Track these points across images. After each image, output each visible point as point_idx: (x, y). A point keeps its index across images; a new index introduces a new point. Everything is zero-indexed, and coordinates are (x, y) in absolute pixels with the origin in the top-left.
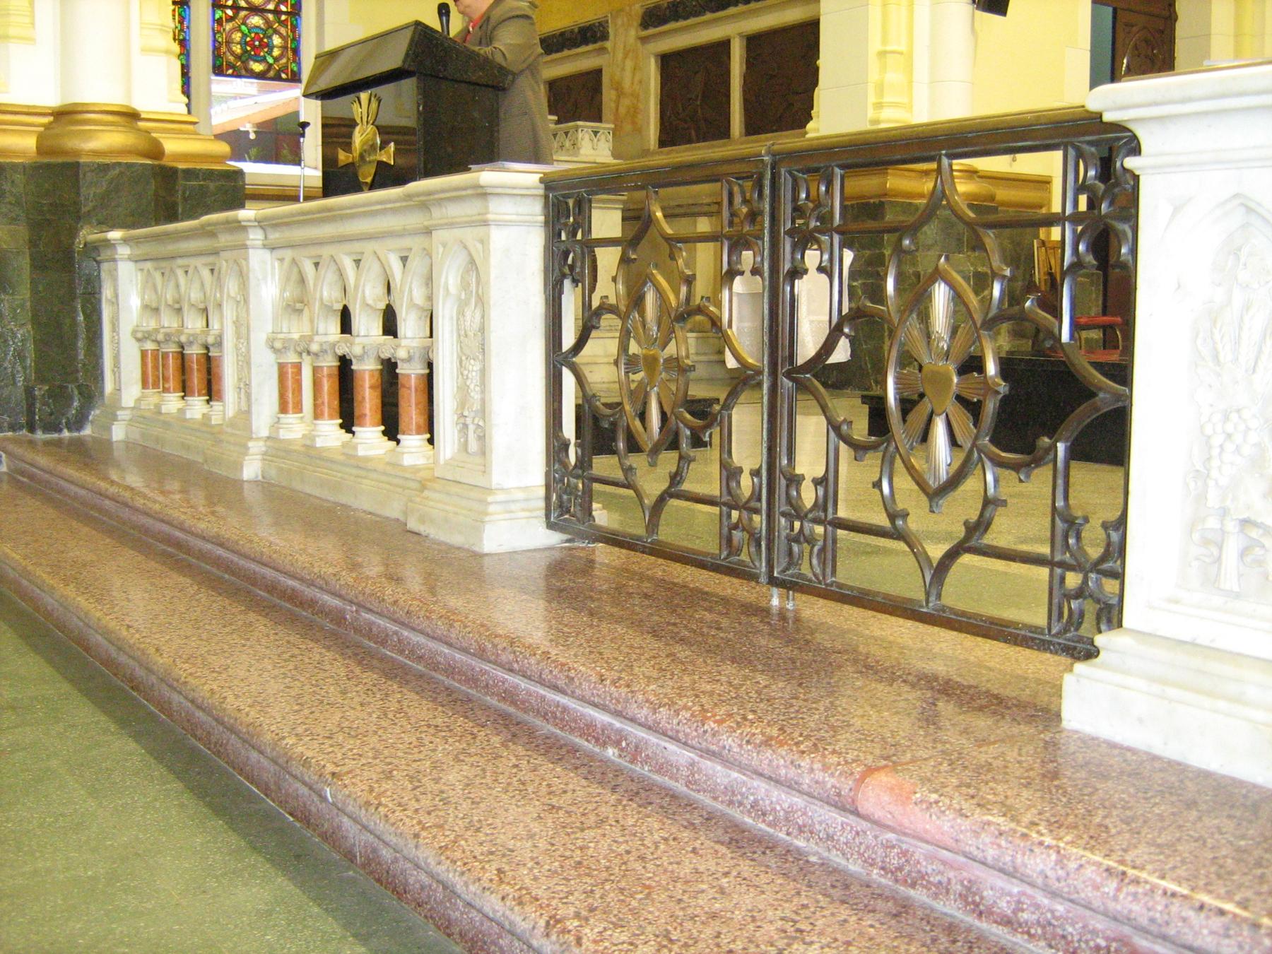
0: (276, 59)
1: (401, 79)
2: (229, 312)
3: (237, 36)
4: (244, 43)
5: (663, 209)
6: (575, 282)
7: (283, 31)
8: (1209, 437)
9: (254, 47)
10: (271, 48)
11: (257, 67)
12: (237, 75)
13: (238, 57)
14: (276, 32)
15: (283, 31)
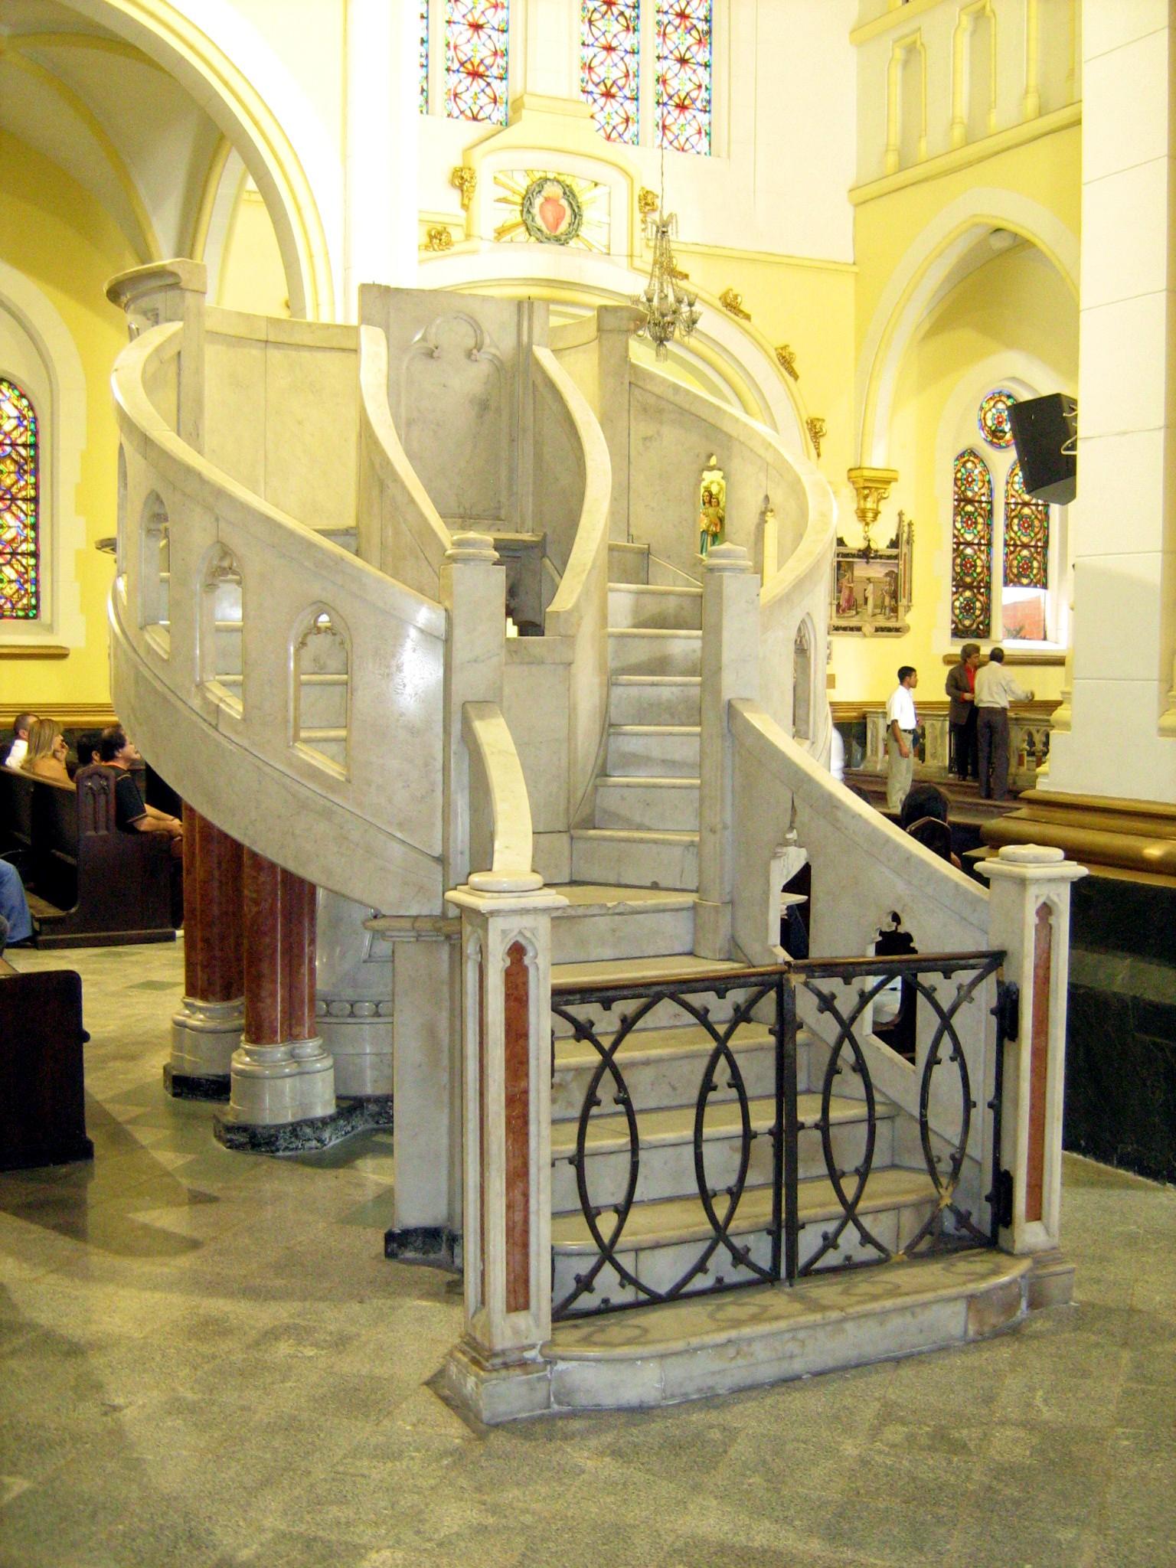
0: (1035, 576)
1: (187, 971)
2: (408, 1021)
3: (1015, 563)
4: (1018, 567)
5: (162, 571)
6: (892, 727)
7: (1038, 558)
8: (616, 1209)
9: (1024, 569)
10: (1032, 568)
11: (1025, 581)
12: (1015, 585)
13: (1016, 576)
14: (1035, 559)
15: (1038, 558)
